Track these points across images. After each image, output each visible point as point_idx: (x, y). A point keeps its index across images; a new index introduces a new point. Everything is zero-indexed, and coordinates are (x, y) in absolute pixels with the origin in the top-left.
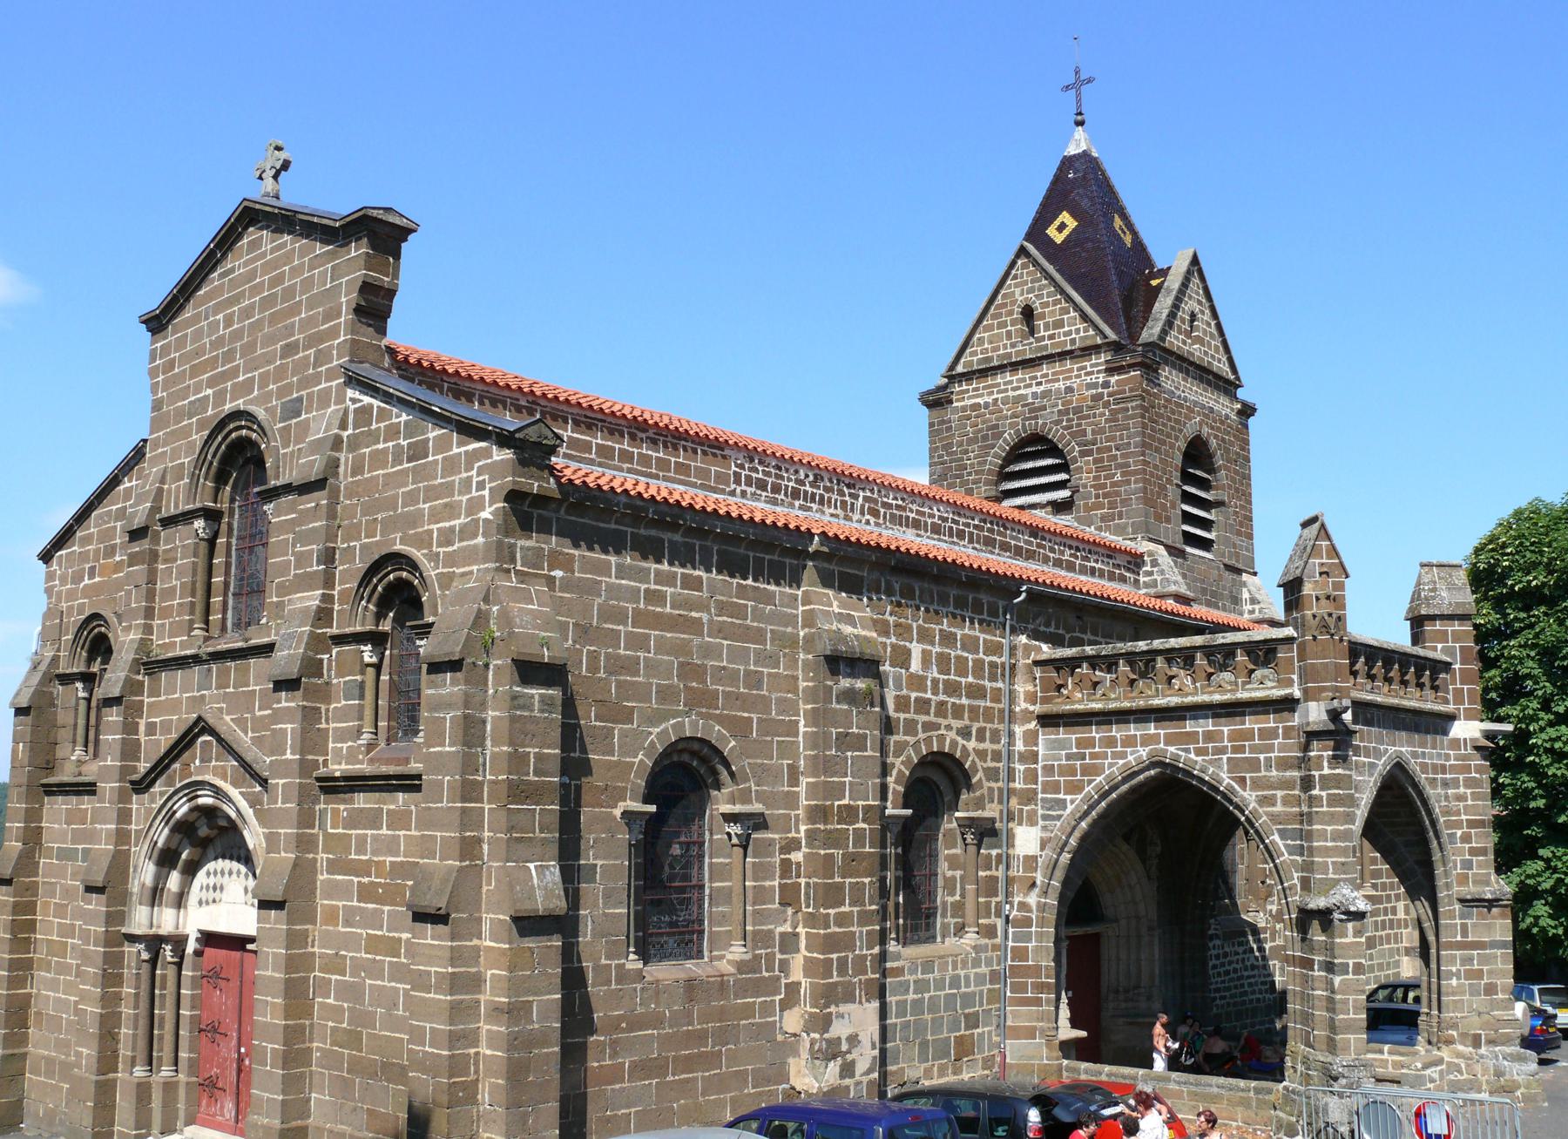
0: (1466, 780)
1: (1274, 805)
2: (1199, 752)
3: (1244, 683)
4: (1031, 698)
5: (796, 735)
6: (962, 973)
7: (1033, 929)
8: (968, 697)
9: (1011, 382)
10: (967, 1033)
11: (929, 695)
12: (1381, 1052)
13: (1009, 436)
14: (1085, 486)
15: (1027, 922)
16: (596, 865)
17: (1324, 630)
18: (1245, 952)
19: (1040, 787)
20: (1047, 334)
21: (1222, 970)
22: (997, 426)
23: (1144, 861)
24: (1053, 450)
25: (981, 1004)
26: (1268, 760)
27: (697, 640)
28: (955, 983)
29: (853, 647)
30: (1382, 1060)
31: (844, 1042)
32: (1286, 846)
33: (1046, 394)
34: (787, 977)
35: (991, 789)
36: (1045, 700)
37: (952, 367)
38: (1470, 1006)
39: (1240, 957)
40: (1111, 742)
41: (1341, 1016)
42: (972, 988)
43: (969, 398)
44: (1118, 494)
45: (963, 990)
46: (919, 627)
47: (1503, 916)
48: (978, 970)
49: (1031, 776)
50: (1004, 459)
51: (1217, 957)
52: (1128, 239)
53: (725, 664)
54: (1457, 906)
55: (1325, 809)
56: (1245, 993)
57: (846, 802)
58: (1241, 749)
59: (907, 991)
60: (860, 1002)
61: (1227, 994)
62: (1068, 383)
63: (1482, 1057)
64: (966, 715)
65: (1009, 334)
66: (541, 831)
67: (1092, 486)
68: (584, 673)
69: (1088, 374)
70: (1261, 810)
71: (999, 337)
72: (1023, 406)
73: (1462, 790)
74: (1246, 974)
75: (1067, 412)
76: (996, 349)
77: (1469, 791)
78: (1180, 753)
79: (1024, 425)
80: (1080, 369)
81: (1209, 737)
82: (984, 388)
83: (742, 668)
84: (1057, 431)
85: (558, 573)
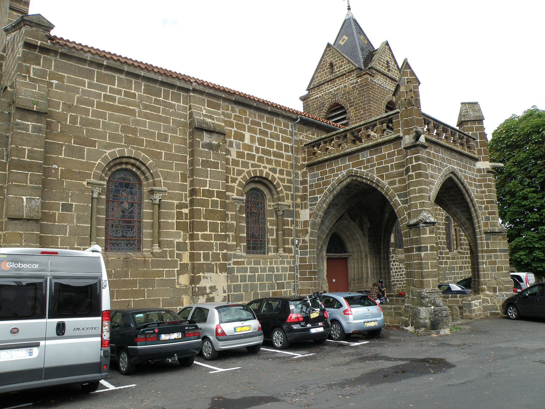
0: (485, 185)
1: (395, 184)
2: (365, 168)
3: (381, 136)
4: (304, 159)
5: (186, 161)
6: (275, 266)
7: (308, 250)
8: (274, 156)
10: (278, 290)
11: (254, 153)
12: (456, 297)
14: (352, 117)
15: (306, 247)
16: (72, 204)
19: (308, 193)
22: (323, 103)
24: (342, 108)
26: (392, 165)
27: (132, 118)
28: (271, 269)
29: (210, 126)
30: (457, 300)
31: (208, 289)
33: (338, 89)
34: (181, 260)
36: (309, 160)
37: (308, 87)
41: (425, 270)
42: (280, 273)
45: (276, 273)
46: (248, 126)
47: (504, 239)
48: (283, 266)
49: (305, 190)
52: (366, 42)
53: (147, 129)
55: (415, 180)
57: (207, 188)
58: (381, 163)
59: (246, 272)
60: (217, 273)
63: (497, 296)
64: (274, 163)
65: (326, 73)
66: (31, 183)
68: (68, 123)
73: (483, 189)
75: (345, 94)
77: (486, 189)
78: (358, 170)
81: (369, 161)
82: (319, 92)
83: (157, 132)
84: (342, 100)
85: (55, 82)
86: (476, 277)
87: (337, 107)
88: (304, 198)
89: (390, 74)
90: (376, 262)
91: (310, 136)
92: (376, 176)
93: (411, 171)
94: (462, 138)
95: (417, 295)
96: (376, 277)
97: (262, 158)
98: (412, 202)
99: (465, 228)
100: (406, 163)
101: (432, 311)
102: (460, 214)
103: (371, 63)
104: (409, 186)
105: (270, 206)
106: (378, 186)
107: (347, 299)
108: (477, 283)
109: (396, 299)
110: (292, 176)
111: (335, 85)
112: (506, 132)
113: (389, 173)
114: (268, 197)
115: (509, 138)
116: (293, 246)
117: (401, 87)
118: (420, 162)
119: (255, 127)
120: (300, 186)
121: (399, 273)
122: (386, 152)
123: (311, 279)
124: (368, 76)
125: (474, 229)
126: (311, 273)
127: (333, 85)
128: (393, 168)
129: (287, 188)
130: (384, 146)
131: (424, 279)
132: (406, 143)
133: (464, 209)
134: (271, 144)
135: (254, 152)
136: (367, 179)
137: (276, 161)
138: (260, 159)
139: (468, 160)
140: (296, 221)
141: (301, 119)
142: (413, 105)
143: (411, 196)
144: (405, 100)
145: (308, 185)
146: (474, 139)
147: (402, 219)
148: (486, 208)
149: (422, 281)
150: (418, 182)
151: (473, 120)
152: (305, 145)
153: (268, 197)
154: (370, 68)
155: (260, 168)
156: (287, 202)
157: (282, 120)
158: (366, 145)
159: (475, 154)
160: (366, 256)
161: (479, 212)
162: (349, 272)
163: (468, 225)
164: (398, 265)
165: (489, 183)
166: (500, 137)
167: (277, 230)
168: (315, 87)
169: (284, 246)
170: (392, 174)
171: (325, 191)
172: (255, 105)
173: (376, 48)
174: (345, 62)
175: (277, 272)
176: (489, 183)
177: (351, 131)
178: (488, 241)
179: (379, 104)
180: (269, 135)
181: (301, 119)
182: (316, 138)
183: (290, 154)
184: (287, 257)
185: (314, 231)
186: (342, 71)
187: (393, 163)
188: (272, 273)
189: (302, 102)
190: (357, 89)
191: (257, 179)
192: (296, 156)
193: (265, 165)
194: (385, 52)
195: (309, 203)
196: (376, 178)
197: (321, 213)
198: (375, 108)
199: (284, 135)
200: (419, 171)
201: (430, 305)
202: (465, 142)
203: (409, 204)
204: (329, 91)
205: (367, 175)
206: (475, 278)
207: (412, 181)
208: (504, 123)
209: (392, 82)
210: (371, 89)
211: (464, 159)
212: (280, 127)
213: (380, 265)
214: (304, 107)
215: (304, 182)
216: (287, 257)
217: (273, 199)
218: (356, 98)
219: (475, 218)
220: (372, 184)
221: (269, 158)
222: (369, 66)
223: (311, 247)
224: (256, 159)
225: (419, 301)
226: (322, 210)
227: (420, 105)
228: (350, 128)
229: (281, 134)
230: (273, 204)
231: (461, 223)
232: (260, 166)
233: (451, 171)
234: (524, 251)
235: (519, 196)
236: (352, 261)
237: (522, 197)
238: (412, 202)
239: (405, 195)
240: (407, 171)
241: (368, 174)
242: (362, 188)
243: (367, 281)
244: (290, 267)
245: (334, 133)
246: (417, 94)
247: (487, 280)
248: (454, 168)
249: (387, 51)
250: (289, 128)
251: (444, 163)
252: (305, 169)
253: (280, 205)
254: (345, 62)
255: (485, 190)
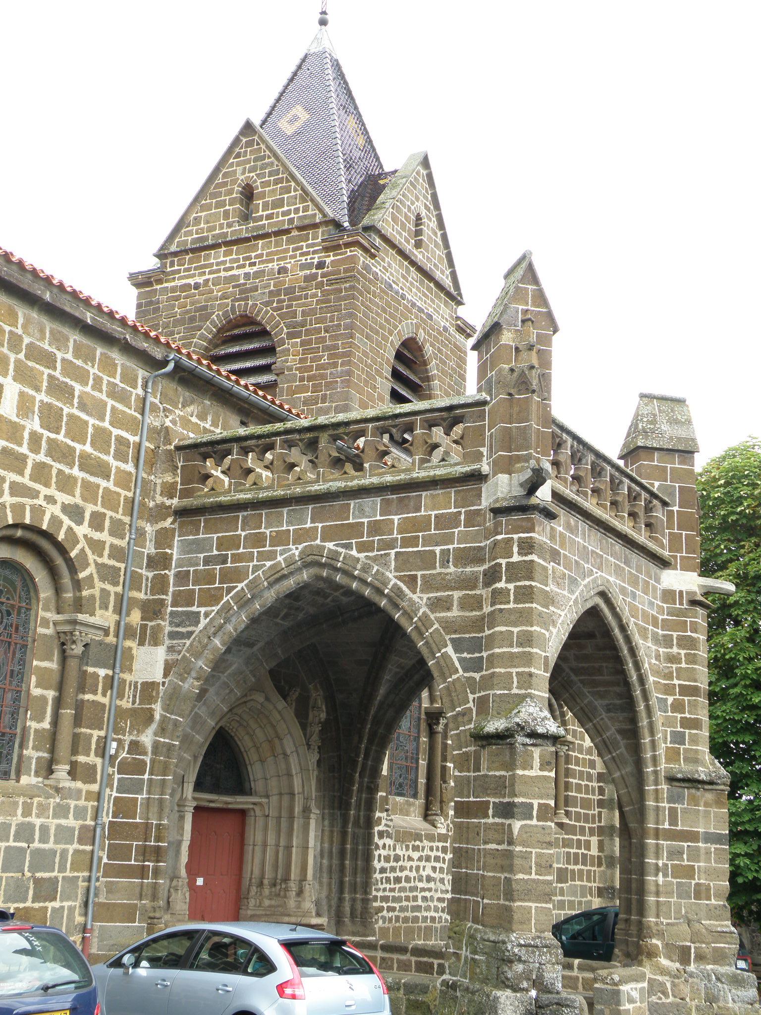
0: (679, 638)
1: (449, 609)
2: (362, 548)
4: (169, 490)
6: (38, 822)
7: (146, 776)
8: (81, 469)
9: (224, 262)
10: (37, 905)
11: (24, 449)
13: (217, 317)
15: (139, 767)
17: (523, 387)
18: (420, 859)
20: (265, 213)
21: (392, 875)
22: (205, 308)
23: (304, 727)
24: (264, 333)
25: (62, 869)
32: (460, 660)
33: (259, 274)
35: (105, 593)
36: (185, 494)
37: (163, 248)
38: (678, 911)
39: (414, 864)
40: (259, 540)
41: (520, 876)
43: (180, 278)
44: (323, 377)
45: (36, 845)
46: (18, 361)
48: (63, 822)
49: (160, 584)
50: (210, 342)
51: (387, 859)
54: (664, 787)
55: (511, 605)
56: (418, 908)
58: (414, 542)
61: (397, 905)
62: (282, 263)
63: (691, 975)
65: (226, 213)
67: (297, 369)
69: (302, 255)
70: (432, 617)
71: (216, 216)
72: (234, 287)
73: (675, 650)
74: (420, 885)
75: (278, 293)
76: (210, 229)
77: (683, 652)
78: (340, 549)
79: (233, 306)
80: (294, 250)
81: (376, 528)
82: (196, 268)
84: (267, 312)
86: (634, 911)
87: (248, 329)
88: (152, 610)
89: (419, 256)
90: (332, 832)
91: (194, 419)
92: (392, 578)
93: (504, 578)
94: (637, 498)
95: (486, 950)
96: (325, 880)
97: (46, 470)
98: (497, 670)
99: (613, 758)
100: (491, 553)
101: (531, 1004)
102: (604, 715)
103: (372, 212)
104: (492, 619)
105: (45, 623)
106: (396, 606)
107: (289, 946)
108: (633, 930)
109: (383, 959)
110: (127, 539)
111: (249, 258)
112: (728, 484)
113: (434, 575)
114: (45, 592)
115: (732, 501)
116: (99, 761)
117: (505, 332)
118: (534, 557)
119: (38, 366)
120: (143, 572)
121: (392, 875)
122: (433, 510)
123: (142, 872)
124: (359, 252)
125: (639, 763)
126: (144, 852)
127: (245, 259)
128: (448, 562)
129: (108, 574)
130: (428, 493)
131: (514, 901)
132: (500, 495)
133: (618, 702)
134: (77, 430)
135: (25, 445)
136: (363, 581)
137: (86, 485)
138: (41, 473)
139: (644, 562)
140: (119, 678)
141: (178, 367)
142: (534, 391)
143: (497, 650)
144: (512, 370)
145: (173, 572)
146: (665, 504)
147: (459, 714)
148: (678, 707)
149: (509, 909)
150: (521, 612)
151: (668, 450)
152: (178, 448)
153: (45, 592)
154: (366, 229)
155: (36, 501)
156: (102, 616)
157: (119, 358)
158: (375, 480)
159: (662, 546)
160: (306, 810)
161: (659, 716)
162: (248, 857)
163: (623, 750)
164: (389, 849)
165: (693, 635)
166: (708, 497)
167: (58, 703)
168: (186, 252)
169: (74, 758)
170: (443, 579)
171: (225, 599)
172: (47, 297)
173: (387, 168)
174: (293, 193)
175: (40, 841)
176: (693, 635)
177: (331, 432)
178: (676, 805)
179: (379, 344)
180: (76, 401)
181: (178, 367)
182: (219, 433)
183: (130, 467)
184: (78, 794)
185: (173, 717)
186: (281, 219)
187: (451, 547)
188: (25, 845)
189: (134, 292)
190: (320, 285)
191: (19, 533)
192: (145, 476)
193: (52, 491)
194: (415, 187)
195: (168, 629)
196: (392, 583)
197: (202, 664)
198: (365, 354)
199: (120, 406)
200: (527, 583)
201: (525, 984)
202: (643, 509)
203: (484, 673)
204: (230, 273)
205: (366, 569)
206: (629, 911)
207: (502, 607)
208: (724, 458)
209: (422, 283)
210: (361, 294)
211: (636, 558)
212: (112, 380)
213: (343, 842)
214: (139, 306)
215: (159, 561)
216: (78, 794)
217: (57, 601)
218: (313, 312)
219: (646, 732)
220: (376, 598)
221: (67, 471)
222: (366, 221)
223: (155, 769)
224: (28, 471)
225: (494, 971)
226: (208, 654)
227: (549, 392)
228: (333, 420)
229: (110, 402)
230: (59, 617)
231: (604, 741)
232: (35, 494)
233: (601, 588)
234: (746, 843)
235: (745, 676)
236: (260, 822)
237: (752, 679)
238: (497, 670)
239: (476, 645)
240: (492, 576)
241: (370, 567)
242: (333, 601)
243: (300, 893)
244: (82, 827)
245: (279, 426)
246: (545, 360)
247: (665, 921)
248: (608, 581)
249: (423, 184)
250: (135, 387)
251: (586, 566)
252: (170, 520)
253: (82, 624)
254: (293, 193)
255: (679, 654)
